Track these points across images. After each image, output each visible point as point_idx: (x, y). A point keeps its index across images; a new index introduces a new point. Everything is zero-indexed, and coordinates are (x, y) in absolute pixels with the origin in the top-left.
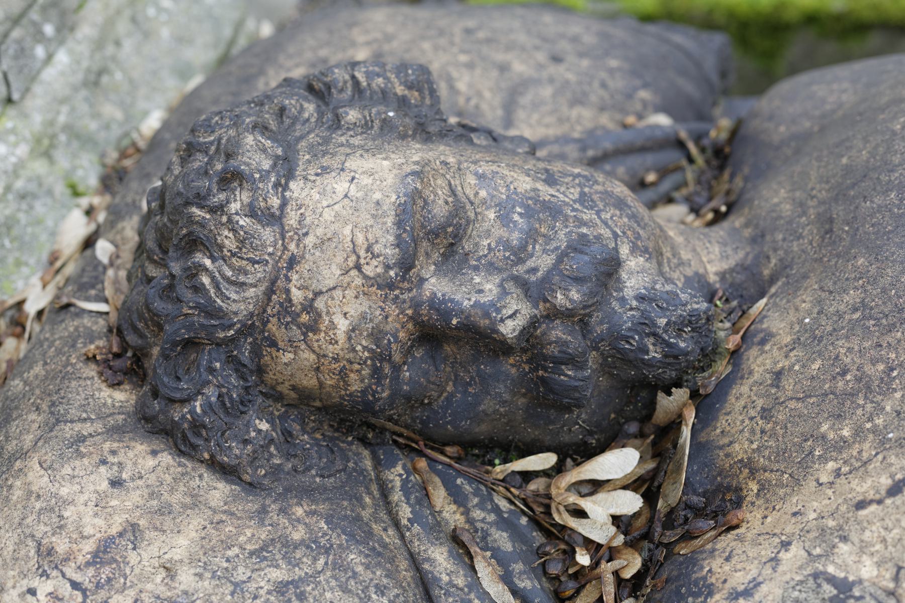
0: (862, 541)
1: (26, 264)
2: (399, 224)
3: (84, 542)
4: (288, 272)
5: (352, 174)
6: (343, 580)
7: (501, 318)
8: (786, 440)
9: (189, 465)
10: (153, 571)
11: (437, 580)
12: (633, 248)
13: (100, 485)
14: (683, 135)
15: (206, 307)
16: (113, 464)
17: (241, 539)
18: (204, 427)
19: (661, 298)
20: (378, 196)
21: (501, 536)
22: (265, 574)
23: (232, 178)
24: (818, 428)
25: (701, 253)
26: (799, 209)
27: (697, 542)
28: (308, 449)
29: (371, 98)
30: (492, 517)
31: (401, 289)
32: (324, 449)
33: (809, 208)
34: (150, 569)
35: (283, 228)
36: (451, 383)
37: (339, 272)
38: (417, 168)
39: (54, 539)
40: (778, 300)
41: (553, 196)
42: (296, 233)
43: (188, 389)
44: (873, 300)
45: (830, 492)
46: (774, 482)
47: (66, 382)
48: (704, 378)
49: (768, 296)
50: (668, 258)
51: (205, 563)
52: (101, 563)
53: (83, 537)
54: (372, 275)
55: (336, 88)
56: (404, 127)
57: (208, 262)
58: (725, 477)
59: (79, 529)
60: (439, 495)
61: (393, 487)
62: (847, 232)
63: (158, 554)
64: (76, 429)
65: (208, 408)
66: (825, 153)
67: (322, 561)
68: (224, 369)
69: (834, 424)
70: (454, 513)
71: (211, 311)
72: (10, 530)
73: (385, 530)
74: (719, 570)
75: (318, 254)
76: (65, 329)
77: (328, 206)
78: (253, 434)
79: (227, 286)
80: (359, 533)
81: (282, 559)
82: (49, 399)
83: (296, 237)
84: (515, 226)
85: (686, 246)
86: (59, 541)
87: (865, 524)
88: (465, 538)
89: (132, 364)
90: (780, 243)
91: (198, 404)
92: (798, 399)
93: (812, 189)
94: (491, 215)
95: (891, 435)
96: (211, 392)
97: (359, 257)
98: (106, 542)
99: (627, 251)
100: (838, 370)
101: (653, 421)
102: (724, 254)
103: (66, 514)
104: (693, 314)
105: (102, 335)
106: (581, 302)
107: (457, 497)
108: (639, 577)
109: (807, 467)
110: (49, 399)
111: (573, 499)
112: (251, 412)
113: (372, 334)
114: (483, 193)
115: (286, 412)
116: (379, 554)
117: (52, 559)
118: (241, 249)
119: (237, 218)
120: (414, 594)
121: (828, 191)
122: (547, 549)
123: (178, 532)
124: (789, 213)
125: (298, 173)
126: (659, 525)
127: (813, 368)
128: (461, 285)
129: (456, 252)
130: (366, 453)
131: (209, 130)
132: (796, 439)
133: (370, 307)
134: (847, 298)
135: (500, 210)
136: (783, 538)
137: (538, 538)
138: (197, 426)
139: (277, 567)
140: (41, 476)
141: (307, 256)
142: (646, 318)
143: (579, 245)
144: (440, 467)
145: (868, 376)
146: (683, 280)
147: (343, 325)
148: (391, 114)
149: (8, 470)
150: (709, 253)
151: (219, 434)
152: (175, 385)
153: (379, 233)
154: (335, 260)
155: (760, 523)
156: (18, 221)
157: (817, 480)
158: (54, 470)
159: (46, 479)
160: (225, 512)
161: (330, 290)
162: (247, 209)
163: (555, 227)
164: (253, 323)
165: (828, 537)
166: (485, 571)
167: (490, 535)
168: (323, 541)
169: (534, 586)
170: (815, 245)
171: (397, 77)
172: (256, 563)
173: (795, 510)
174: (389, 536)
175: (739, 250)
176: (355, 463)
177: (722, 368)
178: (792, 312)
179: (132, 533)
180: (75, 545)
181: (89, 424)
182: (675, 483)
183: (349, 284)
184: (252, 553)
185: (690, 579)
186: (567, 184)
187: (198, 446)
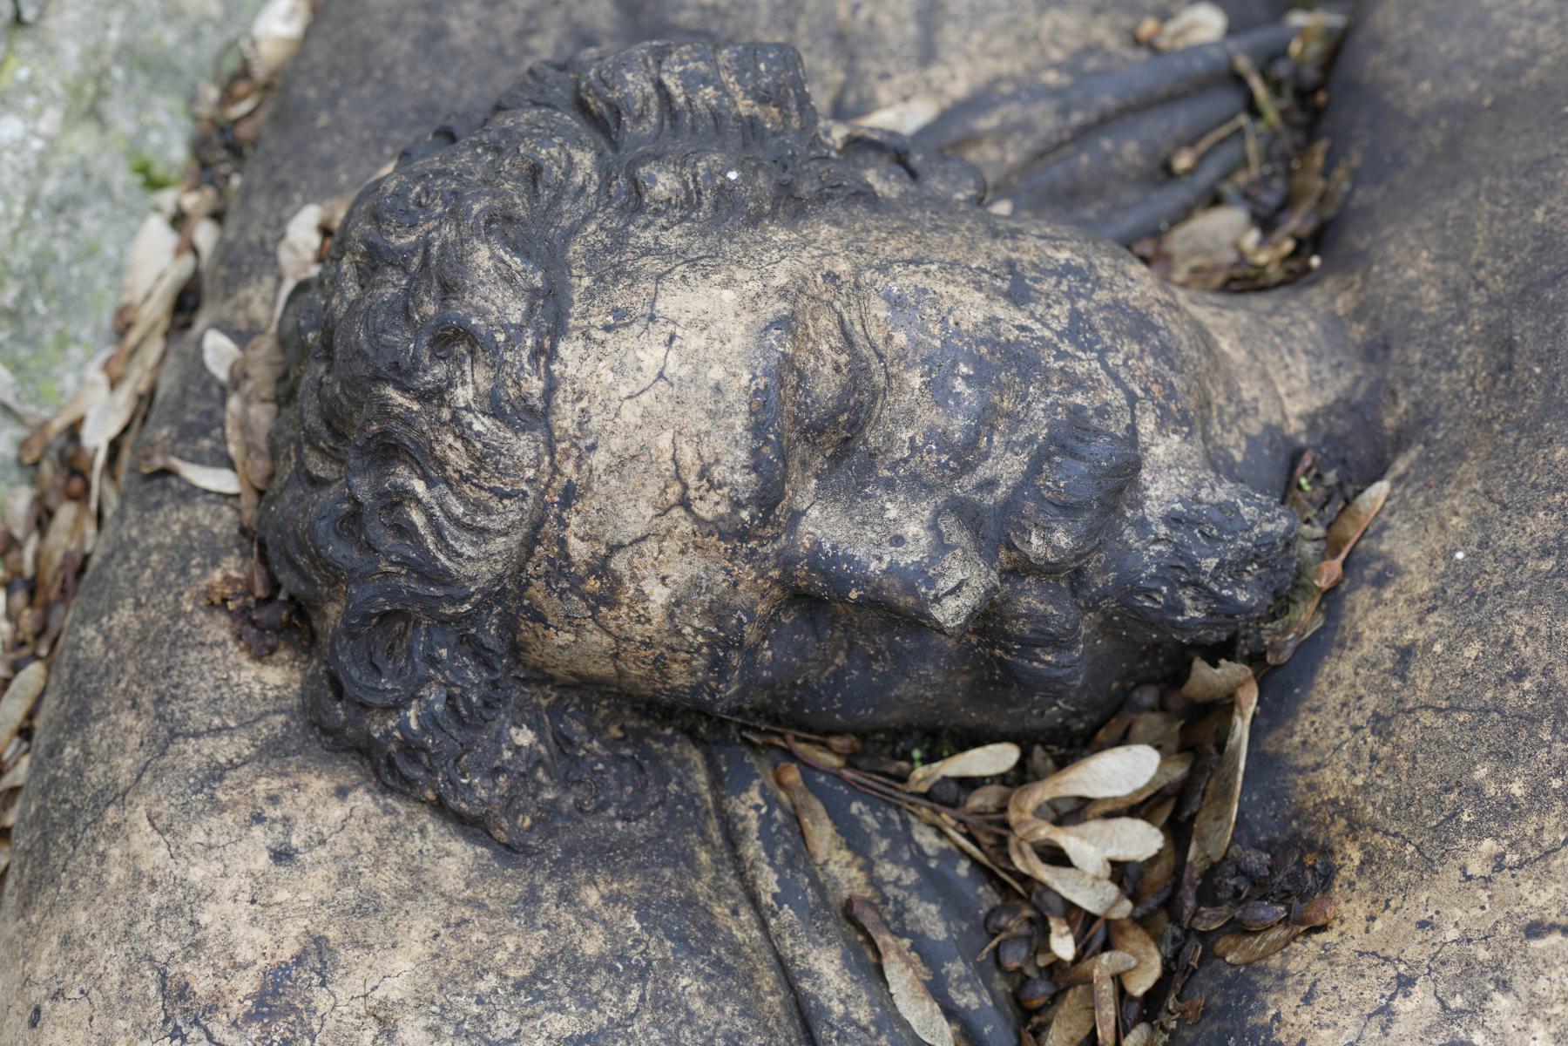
0: (1533, 995)
1: (77, 341)
2: (757, 429)
3: (238, 975)
4: (562, 511)
5: (670, 327)
6: (671, 1027)
7: (936, 596)
8: (1413, 782)
9: (402, 808)
10: (357, 1022)
11: (825, 1011)
12: (1161, 417)
14: (1243, 63)
15: (420, 565)
16: (274, 821)
17: (498, 956)
18: (426, 750)
19: (1210, 519)
20: (717, 373)
21: (927, 911)
22: (543, 1025)
23: (453, 338)
24: (1470, 771)
25: (1275, 378)
26: (1454, 305)
27: (1256, 944)
28: (601, 772)
29: (694, 129)
30: (911, 876)
31: (761, 538)
32: (627, 767)
33: (1472, 306)
34: (351, 1019)
35: (551, 434)
36: (842, 653)
37: (651, 512)
38: (783, 307)
39: (187, 968)
40: (1409, 492)
41: (1023, 328)
42: (574, 445)
43: (393, 690)
45: (1483, 895)
46: (1389, 854)
47: (180, 652)
48: (1275, 632)
49: (1391, 475)
50: (1220, 408)
51: (442, 1007)
52: (270, 1014)
53: (237, 967)
54: (709, 516)
55: (629, 113)
56: (756, 200)
57: (419, 487)
58: (1307, 823)
59: (228, 947)
60: (822, 835)
61: (745, 831)
62: (1538, 377)
63: (361, 991)
64: (206, 751)
65: (430, 721)
66: (1504, 183)
67: (635, 995)
68: (455, 659)
70: (848, 865)
71: (427, 572)
72: (111, 943)
73: (735, 912)
74: (1293, 1020)
75: (613, 482)
76: (165, 525)
77: (630, 397)
78: (507, 755)
79: (456, 533)
80: (691, 930)
81: (570, 994)
82: (153, 687)
83: (575, 452)
84: (958, 404)
85: (1250, 369)
86: (196, 972)
87: (1540, 966)
88: (868, 918)
89: (290, 615)
90: (1417, 370)
91: (412, 713)
93: (1480, 265)
94: (916, 380)
96: (434, 695)
97: (686, 487)
98: (275, 975)
99: (1152, 427)
100: (1509, 668)
101: (1185, 690)
102: (1316, 378)
103: (204, 919)
104: (1267, 541)
105: (231, 543)
106: (1072, 550)
107: (853, 837)
108: (1154, 998)
110: (153, 687)
111: (1046, 832)
112: (502, 716)
113: (710, 610)
114: (900, 338)
115: (560, 699)
116: (729, 971)
117: (187, 1005)
118: (478, 472)
119: (469, 417)
120: (787, 1041)
121: (1507, 277)
122: (1004, 919)
123: (394, 946)
124: (1434, 309)
125: (572, 321)
126: (1191, 893)
127: (1467, 654)
128: (864, 523)
129: (854, 451)
130: (696, 756)
131: (406, 220)
132: (1430, 785)
133: (707, 568)
134: (1532, 526)
135: (931, 371)
136: (1402, 968)
137: (986, 896)
138: (411, 749)
139: (562, 1010)
140: (155, 845)
141: (595, 486)
142: (1181, 559)
143: (1072, 434)
144: (822, 779)
145: (1560, 689)
146: (1243, 444)
147: (659, 596)
148: (733, 175)
149: (95, 821)
150: (1289, 376)
151: (451, 762)
152: (370, 684)
153: (721, 446)
154: (644, 492)
155: (1363, 929)
156: (55, 259)
157: (1463, 869)
158: (175, 834)
159: (163, 851)
160: (468, 902)
161: (637, 541)
162: (487, 402)
164: (504, 588)
165: (1476, 978)
166: (902, 979)
167: (908, 910)
168: (635, 955)
169: (982, 1004)
170: (1479, 388)
171: (738, 81)
172: (526, 1006)
173: (1424, 916)
174: (741, 927)
175: (1342, 370)
176: (680, 784)
177: (1306, 616)
178: (1433, 528)
179: (318, 955)
180: (224, 982)
181: (226, 740)
182: (1218, 818)
183: (669, 531)
184: (519, 985)
185: (1243, 1024)
186: (1048, 296)
187: (416, 780)
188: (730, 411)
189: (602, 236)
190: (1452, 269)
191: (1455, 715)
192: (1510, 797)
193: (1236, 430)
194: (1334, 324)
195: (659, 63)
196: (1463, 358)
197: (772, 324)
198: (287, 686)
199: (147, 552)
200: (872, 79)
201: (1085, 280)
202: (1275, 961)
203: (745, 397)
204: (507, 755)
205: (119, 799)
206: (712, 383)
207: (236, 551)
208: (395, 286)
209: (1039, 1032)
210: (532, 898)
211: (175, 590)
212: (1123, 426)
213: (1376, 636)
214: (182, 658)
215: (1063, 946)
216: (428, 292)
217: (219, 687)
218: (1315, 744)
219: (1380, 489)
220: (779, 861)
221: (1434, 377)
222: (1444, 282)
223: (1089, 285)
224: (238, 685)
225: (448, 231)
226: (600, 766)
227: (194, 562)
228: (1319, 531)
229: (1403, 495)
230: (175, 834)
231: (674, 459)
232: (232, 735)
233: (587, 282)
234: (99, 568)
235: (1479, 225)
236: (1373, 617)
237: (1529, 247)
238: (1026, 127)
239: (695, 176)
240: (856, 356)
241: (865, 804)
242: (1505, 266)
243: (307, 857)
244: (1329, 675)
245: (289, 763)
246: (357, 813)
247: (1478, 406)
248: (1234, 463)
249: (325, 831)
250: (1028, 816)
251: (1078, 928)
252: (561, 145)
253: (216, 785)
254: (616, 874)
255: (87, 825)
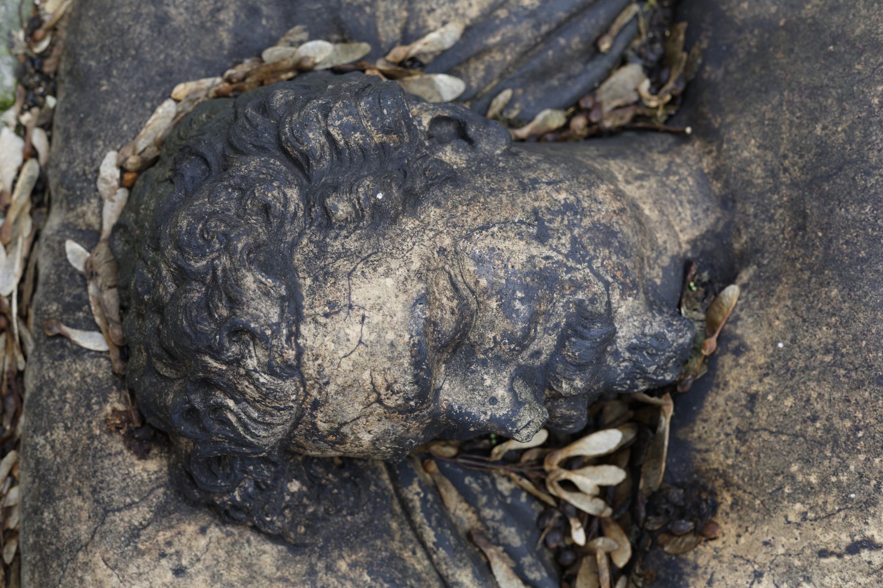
8: (759, 468)
9: (235, 531)
12: (622, 290)
13: (165, 577)
16: (171, 555)
19: (651, 346)
20: (390, 336)
21: (510, 532)
30: (499, 514)
37: (361, 407)
41: (547, 258)
44: (845, 347)
45: (797, 532)
47: (99, 461)
49: (739, 282)
54: (393, 405)
55: (314, 159)
57: (231, 403)
58: (702, 477)
64: (126, 519)
65: (246, 496)
69: (803, 468)
70: (467, 510)
71: (240, 441)
73: (414, 553)
77: (345, 357)
79: (255, 426)
83: (317, 386)
84: (518, 316)
87: (826, 571)
90: (752, 219)
91: (236, 493)
92: (771, 433)
94: (494, 304)
95: (853, 496)
97: (379, 394)
99: (618, 297)
100: (808, 414)
108: (627, 570)
109: (777, 501)
111: (565, 475)
114: (483, 282)
119: (257, 375)
121: (801, 169)
124: (760, 181)
125: (305, 310)
127: (786, 404)
128: (474, 390)
131: (198, 252)
132: (768, 471)
135: (501, 298)
136: (756, 567)
138: (236, 507)
140: (110, 576)
145: (835, 429)
148: (380, 196)
150: (681, 220)
157: (786, 517)
159: (115, 579)
161: (354, 420)
163: (553, 299)
165: (794, 575)
167: (501, 533)
169: (542, 576)
174: (419, 562)
175: (709, 213)
176: (376, 485)
181: (135, 511)
182: (655, 468)
188: (400, 355)
189: (312, 247)
190: (769, 156)
191: (780, 436)
192: (809, 483)
193: (657, 267)
194: (703, 178)
195: (326, 116)
196: (777, 216)
197: (417, 301)
198: (161, 470)
199: (63, 391)
200: (424, 13)
201: (576, 213)
202: (690, 556)
203: (408, 348)
204: (288, 498)
205: (84, 548)
206: (389, 342)
207: (114, 387)
208: (199, 292)
209: (571, 579)
210: (312, 572)
211: (87, 420)
212: (604, 304)
213: (736, 385)
214: (101, 464)
215: (579, 536)
216: (221, 300)
217: (124, 480)
218: (705, 439)
219: (732, 292)
220: (434, 524)
221: (761, 224)
222: (765, 164)
223: (579, 217)
224: (135, 476)
225: (225, 260)
226: (336, 491)
227: (93, 401)
228: (702, 316)
229: (747, 297)
230: (120, 570)
231: (372, 383)
232: (138, 507)
233: (308, 281)
234: (34, 395)
235: (784, 128)
236: (734, 373)
237: (813, 152)
238: (516, 39)
239: (359, 199)
240: (461, 298)
241: (472, 476)
242: (800, 161)
243: (191, 570)
244: (711, 402)
245: (172, 519)
246: (214, 540)
247: (787, 247)
248: (657, 286)
249: (199, 553)
250: (555, 467)
251: (585, 523)
252: (279, 187)
253: (137, 540)
254: (353, 549)
255: (68, 561)
